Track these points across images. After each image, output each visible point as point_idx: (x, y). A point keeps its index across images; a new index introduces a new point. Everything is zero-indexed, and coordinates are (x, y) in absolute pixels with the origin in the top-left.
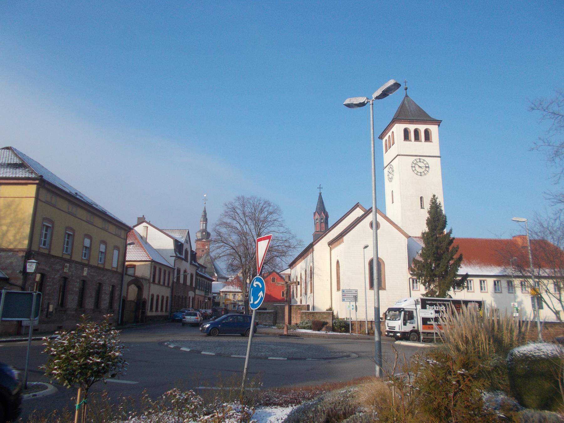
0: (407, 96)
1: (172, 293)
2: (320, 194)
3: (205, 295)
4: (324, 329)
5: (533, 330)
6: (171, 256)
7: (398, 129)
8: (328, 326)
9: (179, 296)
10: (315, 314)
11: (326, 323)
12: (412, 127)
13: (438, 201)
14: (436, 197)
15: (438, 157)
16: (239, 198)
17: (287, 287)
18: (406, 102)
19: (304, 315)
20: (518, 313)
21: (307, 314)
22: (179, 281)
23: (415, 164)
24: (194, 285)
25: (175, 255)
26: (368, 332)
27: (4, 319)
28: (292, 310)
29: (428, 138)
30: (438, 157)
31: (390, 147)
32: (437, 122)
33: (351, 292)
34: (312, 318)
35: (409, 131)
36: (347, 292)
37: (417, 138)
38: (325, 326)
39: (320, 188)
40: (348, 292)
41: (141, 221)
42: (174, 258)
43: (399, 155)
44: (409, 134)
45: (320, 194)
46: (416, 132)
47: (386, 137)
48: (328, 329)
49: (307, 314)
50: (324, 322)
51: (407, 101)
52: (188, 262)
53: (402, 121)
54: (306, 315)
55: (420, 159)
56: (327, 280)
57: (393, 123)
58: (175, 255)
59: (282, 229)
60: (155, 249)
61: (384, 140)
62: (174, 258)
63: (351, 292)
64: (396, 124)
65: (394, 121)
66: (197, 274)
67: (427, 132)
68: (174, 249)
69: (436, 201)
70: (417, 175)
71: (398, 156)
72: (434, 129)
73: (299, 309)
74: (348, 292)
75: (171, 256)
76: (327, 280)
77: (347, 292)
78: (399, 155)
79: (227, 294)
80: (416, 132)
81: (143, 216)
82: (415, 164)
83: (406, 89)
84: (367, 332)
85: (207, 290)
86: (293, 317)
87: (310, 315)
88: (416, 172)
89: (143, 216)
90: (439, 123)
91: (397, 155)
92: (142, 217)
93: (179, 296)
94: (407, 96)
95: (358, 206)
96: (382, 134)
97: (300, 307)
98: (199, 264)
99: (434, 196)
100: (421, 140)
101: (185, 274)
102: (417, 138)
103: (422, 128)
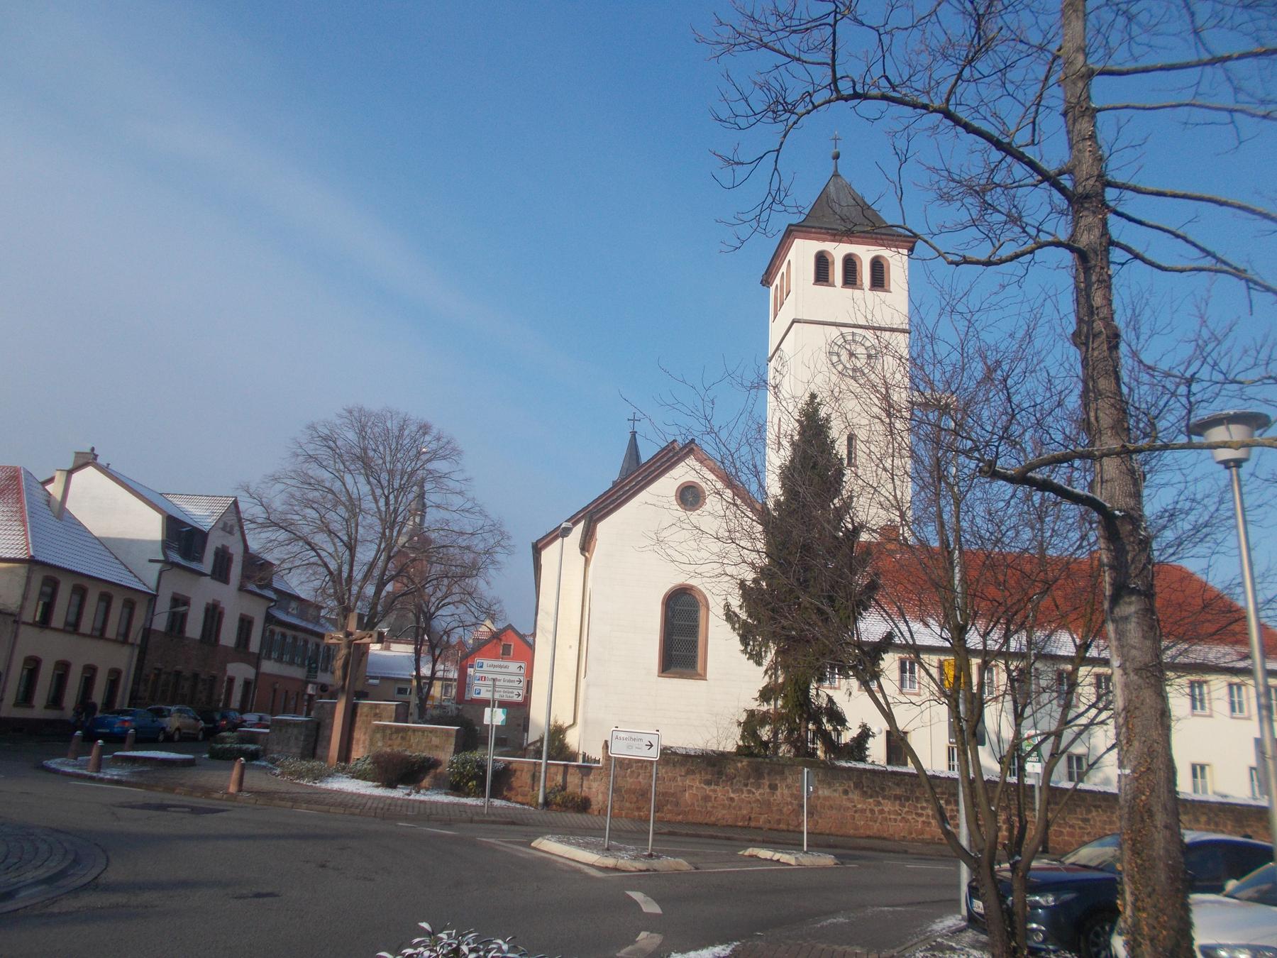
0: (836, 175)
1: (141, 660)
2: (634, 434)
3: (307, 677)
4: (426, 782)
5: (1090, 816)
6: (151, 561)
7: (803, 252)
8: (440, 773)
9: (196, 676)
10: (410, 733)
11: (436, 764)
12: (838, 251)
13: (823, 413)
14: (818, 400)
15: (903, 331)
16: (350, 412)
17: (349, 647)
18: (832, 189)
19: (378, 736)
20: (1039, 761)
21: (388, 732)
22: (182, 630)
23: (839, 346)
24: (254, 646)
25: (161, 557)
26: (545, 798)
27: (1074, 758)
28: (358, 719)
29: (879, 278)
30: (903, 331)
31: (782, 304)
32: (908, 241)
33: (503, 670)
34: (400, 745)
35: (830, 260)
36: (491, 669)
37: (850, 277)
38: (432, 771)
39: (634, 420)
40: (496, 669)
41: (86, 460)
42: (158, 566)
43: (798, 321)
44: (830, 269)
45: (634, 434)
46: (850, 264)
47: (777, 281)
48: (438, 786)
49: (388, 732)
50: (429, 759)
51: (835, 186)
52: (759, 664)
53: (811, 232)
54: (384, 737)
55: (853, 334)
56: (570, 647)
57: (788, 238)
58: (161, 557)
59: (457, 501)
60: (96, 538)
61: (773, 288)
62: (158, 566)
63: (503, 670)
64: (796, 240)
65: (791, 231)
66: (269, 619)
67: (878, 268)
68: (163, 541)
69: (816, 411)
70: (843, 375)
71: (795, 324)
72: (897, 262)
73: (376, 715)
74: (496, 669)
75: (151, 561)
76: (570, 647)
77: (491, 669)
78: (798, 321)
79: (451, 685)
80: (850, 264)
81: (93, 449)
82: (839, 346)
83: (836, 157)
84: (541, 800)
85: (314, 665)
86: (358, 740)
87: (394, 736)
88: (840, 367)
89: (93, 449)
90: (909, 242)
91: (794, 322)
92: (88, 450)
93: (178, 673)
94: (836, 175)
95: (691, 451)
96: (768, 269)
97: (378, 711)
98: (277, 591)
99: (813, 396)
100: (862, 285)
101: (174, 610)
102: (850, 277)
103: (865, 253)
